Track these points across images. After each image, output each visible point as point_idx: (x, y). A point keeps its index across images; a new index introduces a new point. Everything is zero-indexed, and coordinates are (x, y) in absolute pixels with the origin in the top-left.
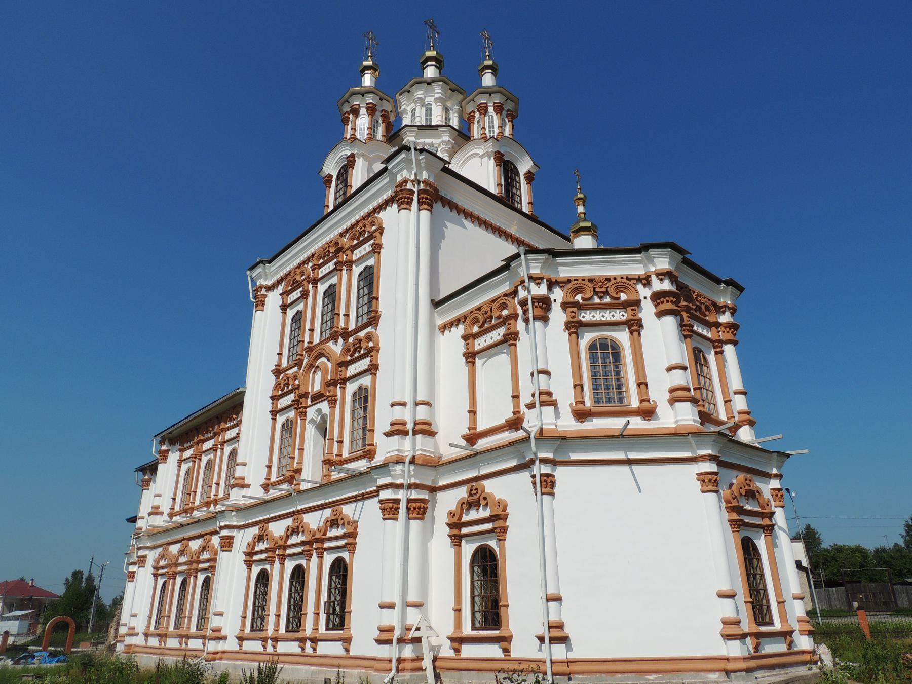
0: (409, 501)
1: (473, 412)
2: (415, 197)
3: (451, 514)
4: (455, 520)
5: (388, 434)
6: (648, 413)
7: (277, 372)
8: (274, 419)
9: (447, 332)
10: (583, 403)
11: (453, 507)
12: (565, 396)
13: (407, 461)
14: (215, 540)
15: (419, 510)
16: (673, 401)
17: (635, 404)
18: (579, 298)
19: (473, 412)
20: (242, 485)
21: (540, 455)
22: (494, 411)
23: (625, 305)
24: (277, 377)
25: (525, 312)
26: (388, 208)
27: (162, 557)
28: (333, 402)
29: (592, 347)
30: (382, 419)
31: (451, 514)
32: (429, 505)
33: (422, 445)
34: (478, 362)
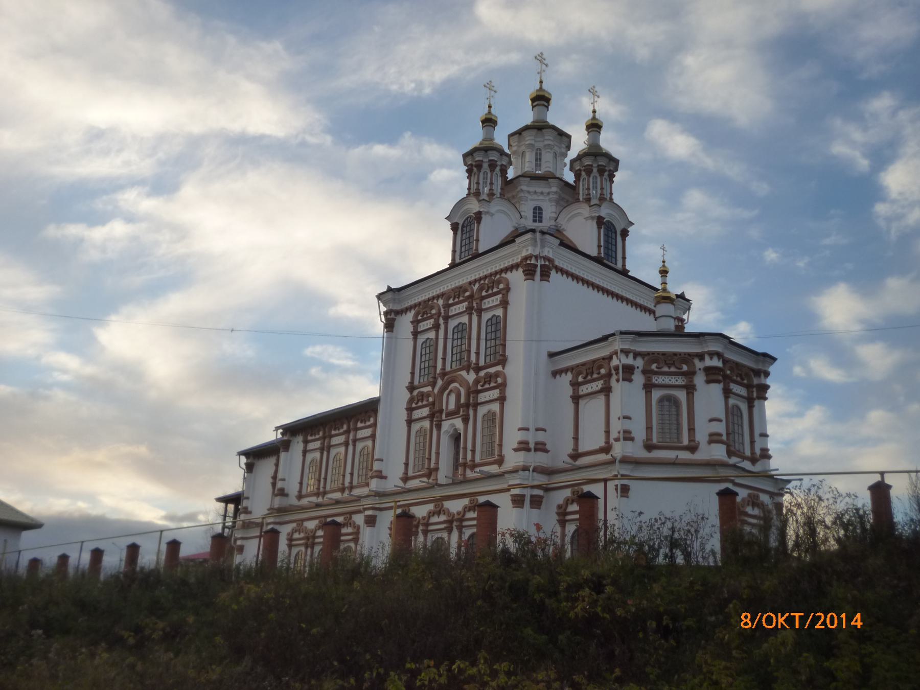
0: (532, 496)
1: (576, 439)
2: (538, 269)
3: (288, 534)
4: (561, 510)
5: (516, 450)
6: (693, 448)
7: (411, 388)
8: (409, 427)
9: (558, 376)
10: (651, 440)
11: (561, 502)
12: (640, 433)
13: (531, 469)
14: (359, 519)
15: (536, 502)
16: (710, 442)
17: (685, 442)
18: (654, 366)
19: (576, 439)
20: (380, 476)
21: (621, 472)
22: (592, 439)
23: (684, 374)
24: (411, 392)
25: (617, 374)
26: (514, 271)
27: (294, 531)
28: (466, 420)
29: (661, 400)
30: (512, 438)
31: (559, 507)
32: (544, 500)
33: (540, 459)
34: (582, 402)
